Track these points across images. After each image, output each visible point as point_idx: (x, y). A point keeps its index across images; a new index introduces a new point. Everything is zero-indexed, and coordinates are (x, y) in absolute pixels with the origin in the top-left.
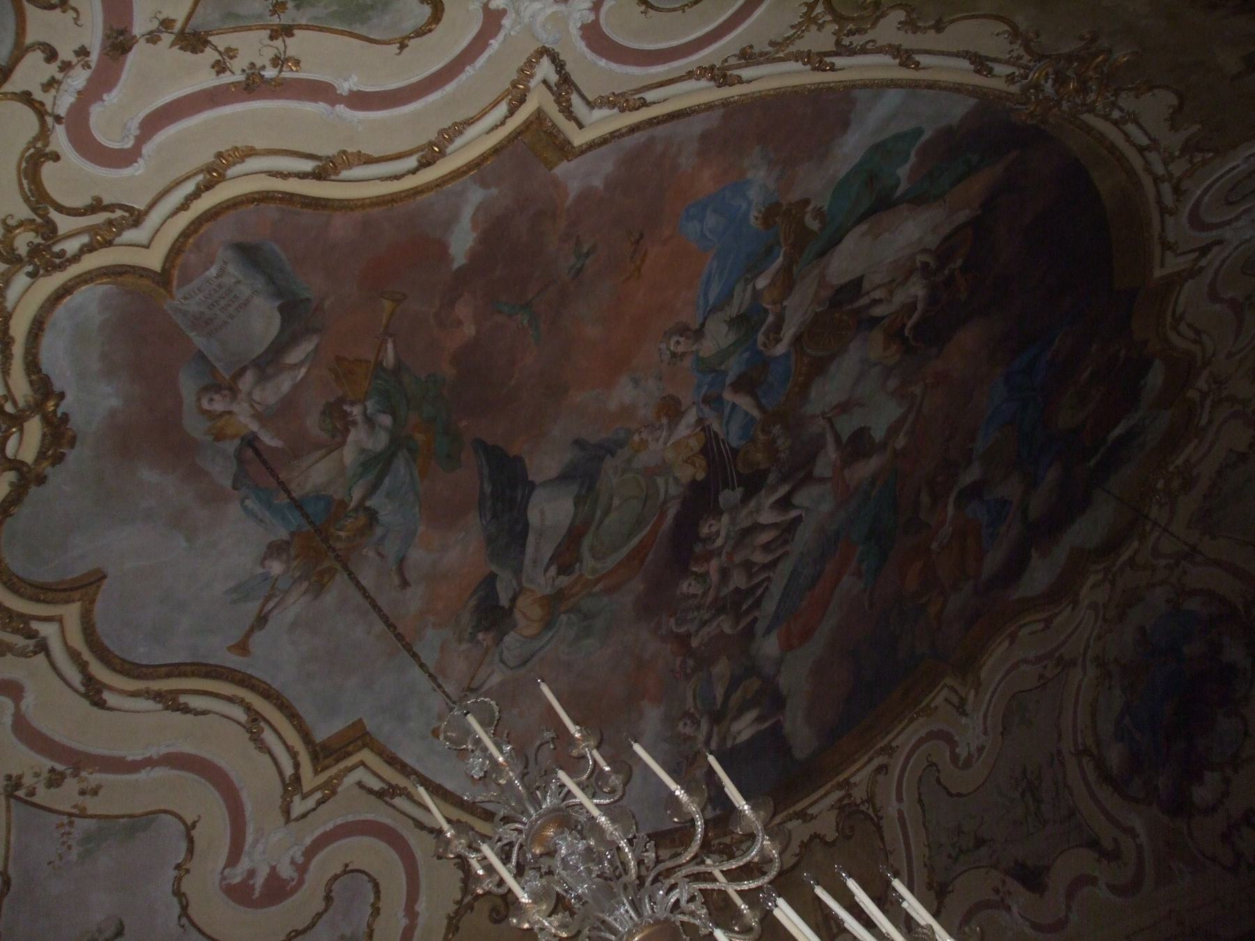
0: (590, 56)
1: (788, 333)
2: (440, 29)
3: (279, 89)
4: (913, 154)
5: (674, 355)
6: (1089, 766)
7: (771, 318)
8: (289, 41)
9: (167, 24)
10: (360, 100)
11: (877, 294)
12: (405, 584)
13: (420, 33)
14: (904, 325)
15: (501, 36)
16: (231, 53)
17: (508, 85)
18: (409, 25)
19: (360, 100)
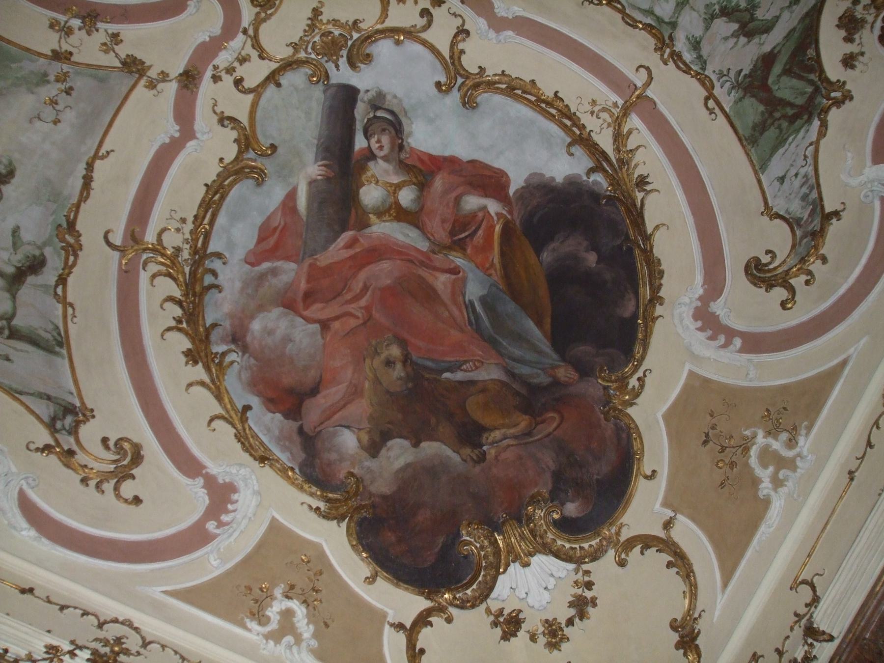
6: (156, 295)
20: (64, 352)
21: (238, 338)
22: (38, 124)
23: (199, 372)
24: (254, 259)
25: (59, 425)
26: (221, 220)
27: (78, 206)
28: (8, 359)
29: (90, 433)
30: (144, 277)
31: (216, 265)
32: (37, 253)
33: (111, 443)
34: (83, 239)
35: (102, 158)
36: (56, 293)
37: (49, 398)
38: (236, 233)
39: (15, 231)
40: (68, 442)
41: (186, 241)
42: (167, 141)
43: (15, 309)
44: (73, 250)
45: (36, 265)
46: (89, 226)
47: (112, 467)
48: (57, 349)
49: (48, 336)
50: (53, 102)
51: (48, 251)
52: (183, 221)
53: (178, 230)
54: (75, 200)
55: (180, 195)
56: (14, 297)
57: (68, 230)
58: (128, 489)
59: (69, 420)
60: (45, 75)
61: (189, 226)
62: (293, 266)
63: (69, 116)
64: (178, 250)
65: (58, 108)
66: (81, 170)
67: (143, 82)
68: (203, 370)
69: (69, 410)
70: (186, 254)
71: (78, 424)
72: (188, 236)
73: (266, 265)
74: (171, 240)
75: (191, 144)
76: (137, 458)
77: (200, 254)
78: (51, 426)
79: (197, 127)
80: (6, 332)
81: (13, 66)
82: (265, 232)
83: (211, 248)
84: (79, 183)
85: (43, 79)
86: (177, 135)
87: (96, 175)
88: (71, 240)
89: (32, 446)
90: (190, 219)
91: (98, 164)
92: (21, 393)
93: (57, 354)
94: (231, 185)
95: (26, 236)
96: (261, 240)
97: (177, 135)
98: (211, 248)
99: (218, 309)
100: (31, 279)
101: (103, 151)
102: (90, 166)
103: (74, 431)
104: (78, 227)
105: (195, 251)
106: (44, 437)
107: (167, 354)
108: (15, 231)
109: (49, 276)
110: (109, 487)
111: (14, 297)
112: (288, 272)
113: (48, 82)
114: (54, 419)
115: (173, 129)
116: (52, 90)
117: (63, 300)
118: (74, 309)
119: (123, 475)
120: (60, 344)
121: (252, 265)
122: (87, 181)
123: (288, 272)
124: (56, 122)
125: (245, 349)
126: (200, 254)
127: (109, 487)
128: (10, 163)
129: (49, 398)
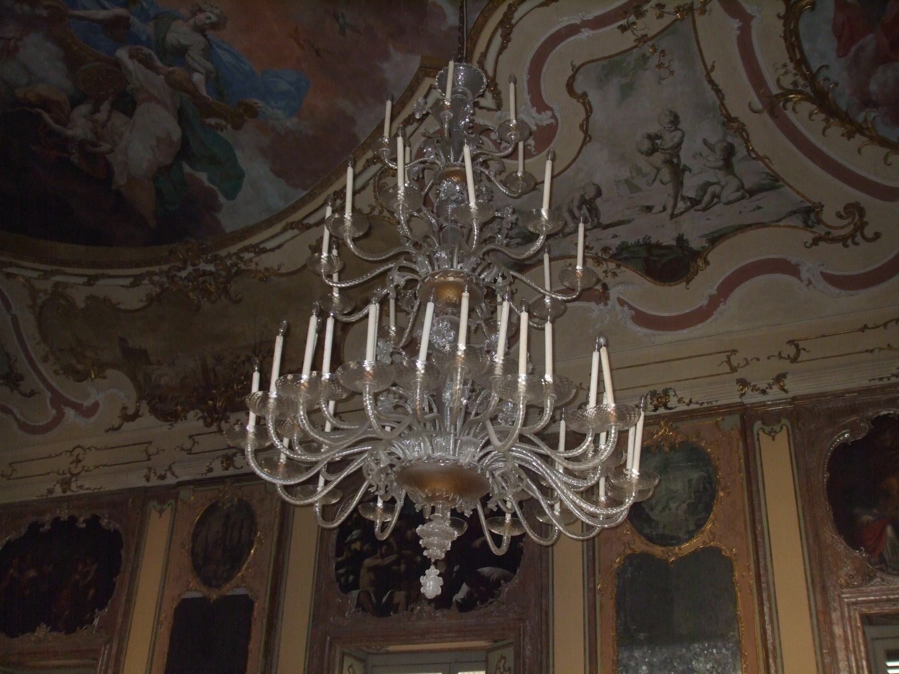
0: (594, 32)
1: (131, 65)
2: (748, 109)
3: (623, 12)
4: (211, 185)
5: (201, 10)
6: (803, 115)
7: (159, 64)
8: (635, 38)
9: (703, 11)
10: (572, 30)
11: (102, 116)
12: (870, 380)
13: (572, 78)
14: (49, 112)
15: (528, 101)
16: (660, 16)
17: (497, 81)
18: (579, 78)
19: (572, 30)
20: (781, 183)
21: (867, 102)
22: (664, 82)
23: (859, 139)
24: (842, 51)
25: (810, 223)
26: (806, 46)
27: (723, 105)
28: (759, 208)
29: (829, 215)
30: (789, 113)
31: (824, 73)
32: (725, 144)
33: (843, 213)
34: (741, 119)
35: (712, 70)
36: (753, 158)
37: (795, 212)
38: (821, 47)
39: (705, 142)
40: (821, 230)
41: (796, 74)
42: (738, 32)
43: (741, 181)
44: (741, 130)
45: (729, 152)
46: (736, 109)
47: (852, 227)
48: (777, 184)
49: (767, 181)
50: (660, 66)
51: (729, 139)
52: (785, 66)
53: (786, 73)
54: (718, 102)
55: (772, 54)
56: (734, 175)
57: (729, 120)
58: (869, 232)
59: (812, 216)
60: (644, 55)
61: (791, 66)
62: (871, 36)
63: (676, 65)
64: (795, 84)
65: (666, 65)
66: (708, 87)
67: (696, 14)
68: (861, 137)
69: (808, 211)
70: (801, 82)
71: (817, 214)
72: (794, 71)
73: (853, 50)
74: (787, 82)
75: (754, 23)
76: (861, 212)
77: (811, 78)
78: (807, 226)
79: (749, 11)
80: (747, 195)
81: (624, 65)
82: (838, 32)
83: (814, 70)
84: (713, 93)
85: (645, 58)
86: (741, 24)
87: (717, 82)
88: (735, 125)
89: (808, 245)
90: (788, 61)
91: (713, 74)
92: (779, 221)
93: (779, 187)
94: (796, 26)
95: (713, 140)
96: (839, 38)
97: (741, 24)
98: (814, 70)
99: (844, 99)
100: (734, 160)
101: (709, 67)
102: (711, 81)
103: (820, 222)
104: (733, 115)
105: (804, 77)
106: (808, 237)
107: (835, 143)
108: (705, 142)
109: (741, 151)
110: (859, 238)
111: (734, 175)
112: (870, 41)
113: (648, 58)
114: (805, 222)
115: (736, 24)
116: (654, 60)
117: (758, 158)
118: (768, 158)
119: (861, 227)
120: (777, 180)
121: (845, 55)
122: (718, 91)
123: (870, 41)
124: (672, 73)
125: (876, 105)
126: (811, 78)
127: (859, 238)
128: (671, 112)
129: (795, 212)
